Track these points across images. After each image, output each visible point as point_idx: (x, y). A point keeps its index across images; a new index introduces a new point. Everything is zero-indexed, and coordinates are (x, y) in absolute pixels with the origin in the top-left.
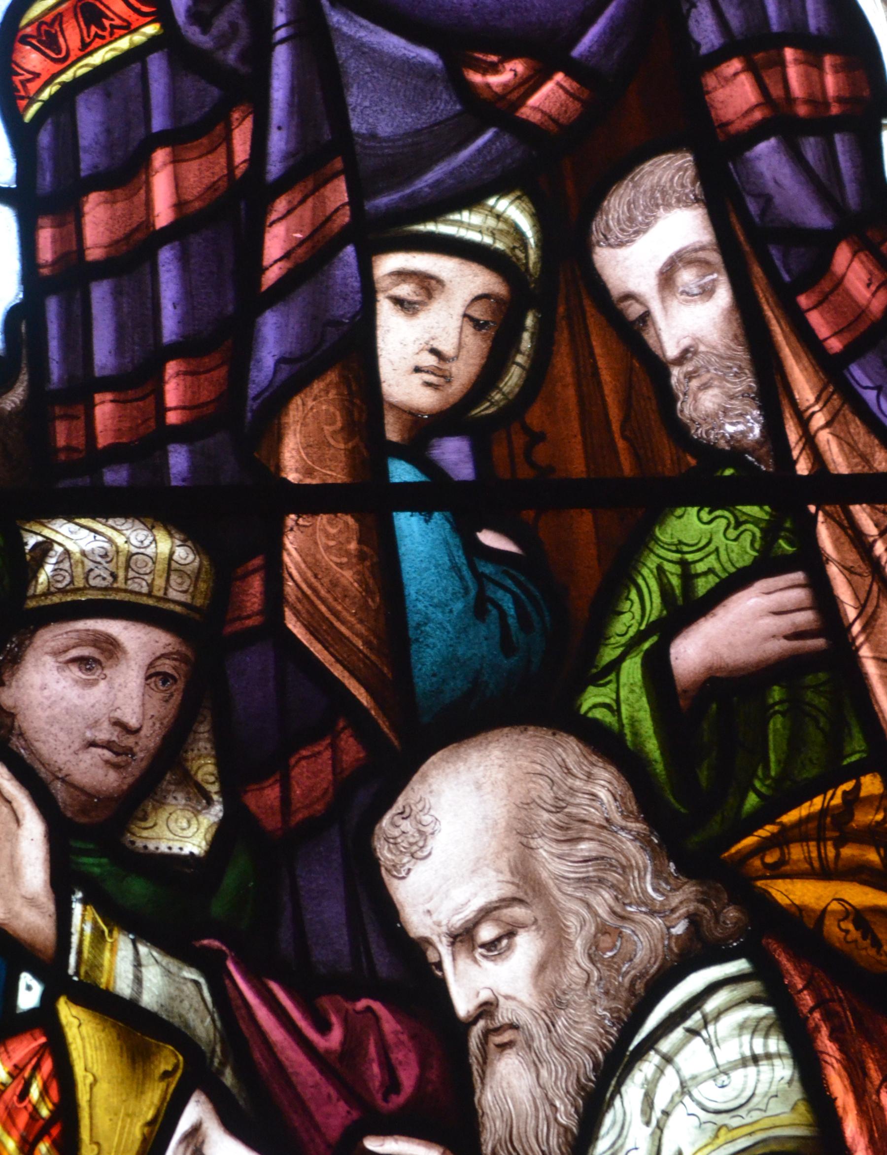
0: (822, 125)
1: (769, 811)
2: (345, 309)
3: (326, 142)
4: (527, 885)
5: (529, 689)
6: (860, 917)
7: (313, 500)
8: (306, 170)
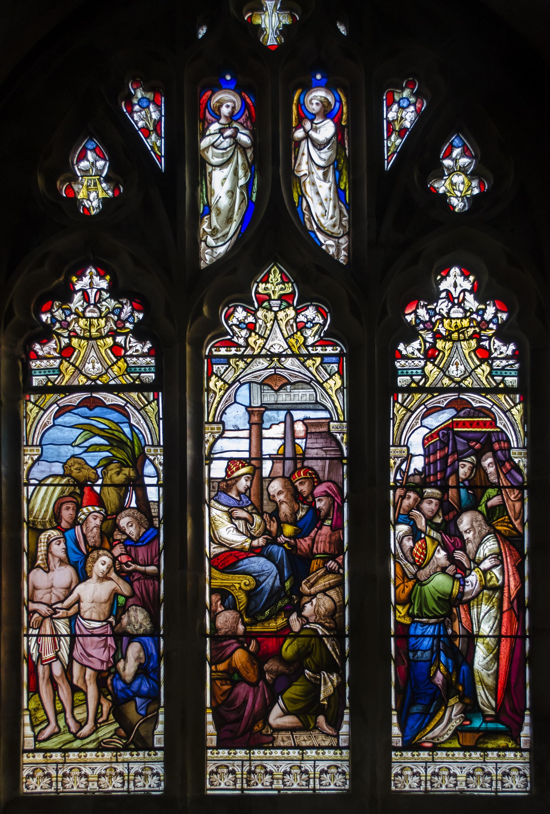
0: (505, 450)
1: (497, 520)
2: (456, 468)
3: (455, 450)
4: (472, 526)
5: (473, 507)
6: (505, 530)
7: (453, 487)
8: (453, 453)
